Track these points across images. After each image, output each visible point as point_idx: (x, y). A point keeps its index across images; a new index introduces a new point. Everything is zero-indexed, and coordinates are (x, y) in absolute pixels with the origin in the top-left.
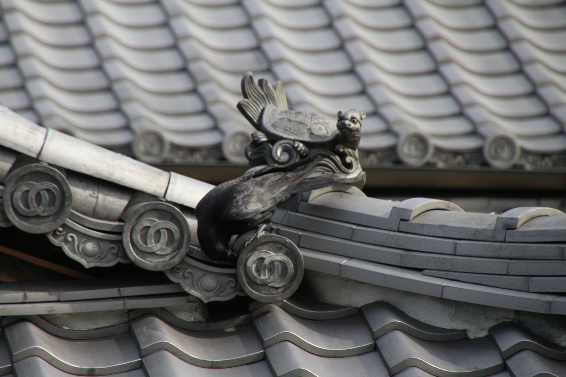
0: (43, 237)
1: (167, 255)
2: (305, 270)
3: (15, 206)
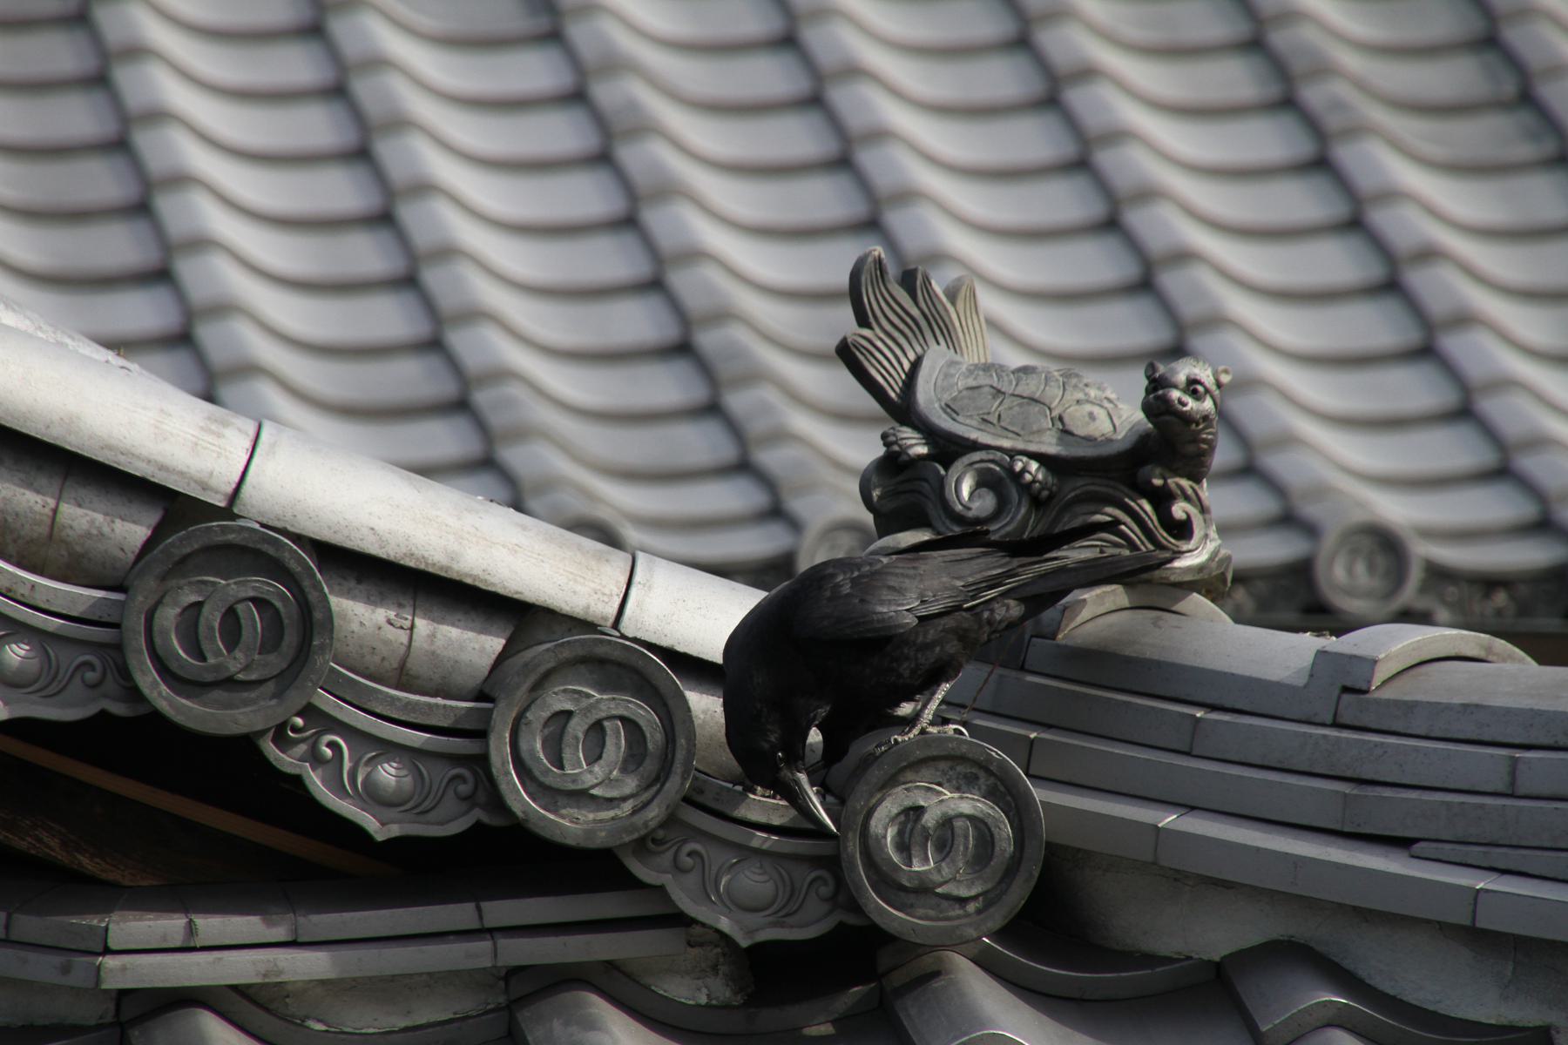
0: (246, 744)
1: (624, 799)
2: (1048, 843)
3: (160, 652)
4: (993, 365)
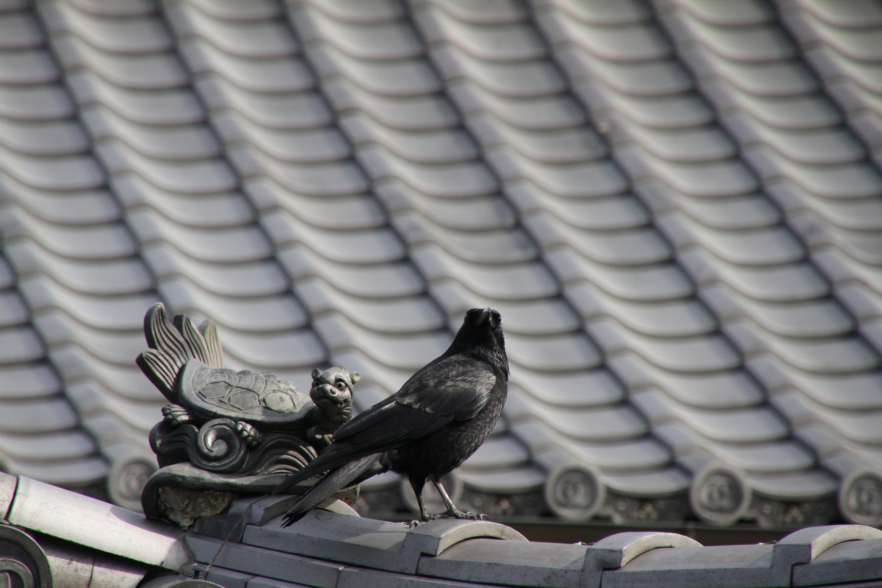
4: (226, 370)
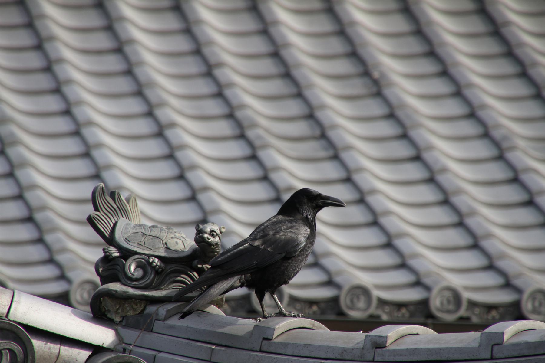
4: (142, 225)
